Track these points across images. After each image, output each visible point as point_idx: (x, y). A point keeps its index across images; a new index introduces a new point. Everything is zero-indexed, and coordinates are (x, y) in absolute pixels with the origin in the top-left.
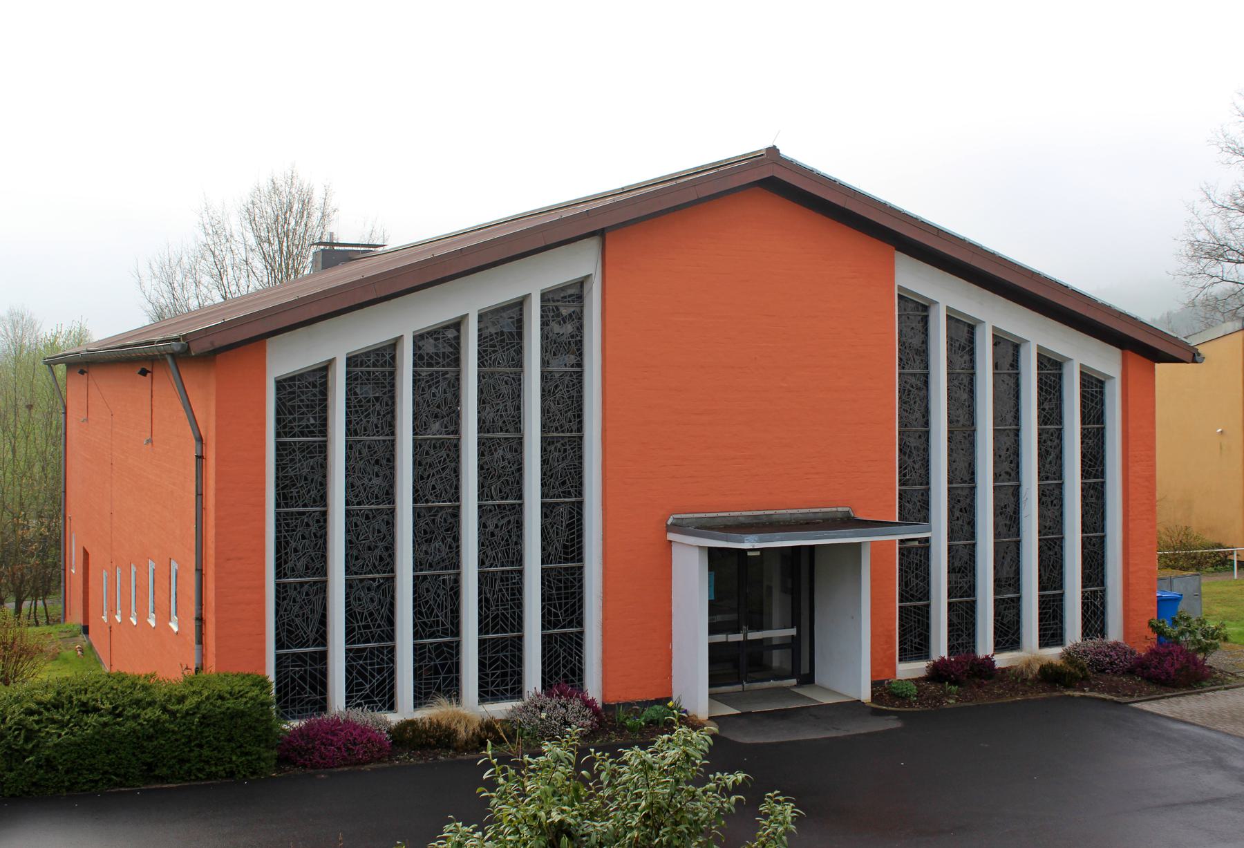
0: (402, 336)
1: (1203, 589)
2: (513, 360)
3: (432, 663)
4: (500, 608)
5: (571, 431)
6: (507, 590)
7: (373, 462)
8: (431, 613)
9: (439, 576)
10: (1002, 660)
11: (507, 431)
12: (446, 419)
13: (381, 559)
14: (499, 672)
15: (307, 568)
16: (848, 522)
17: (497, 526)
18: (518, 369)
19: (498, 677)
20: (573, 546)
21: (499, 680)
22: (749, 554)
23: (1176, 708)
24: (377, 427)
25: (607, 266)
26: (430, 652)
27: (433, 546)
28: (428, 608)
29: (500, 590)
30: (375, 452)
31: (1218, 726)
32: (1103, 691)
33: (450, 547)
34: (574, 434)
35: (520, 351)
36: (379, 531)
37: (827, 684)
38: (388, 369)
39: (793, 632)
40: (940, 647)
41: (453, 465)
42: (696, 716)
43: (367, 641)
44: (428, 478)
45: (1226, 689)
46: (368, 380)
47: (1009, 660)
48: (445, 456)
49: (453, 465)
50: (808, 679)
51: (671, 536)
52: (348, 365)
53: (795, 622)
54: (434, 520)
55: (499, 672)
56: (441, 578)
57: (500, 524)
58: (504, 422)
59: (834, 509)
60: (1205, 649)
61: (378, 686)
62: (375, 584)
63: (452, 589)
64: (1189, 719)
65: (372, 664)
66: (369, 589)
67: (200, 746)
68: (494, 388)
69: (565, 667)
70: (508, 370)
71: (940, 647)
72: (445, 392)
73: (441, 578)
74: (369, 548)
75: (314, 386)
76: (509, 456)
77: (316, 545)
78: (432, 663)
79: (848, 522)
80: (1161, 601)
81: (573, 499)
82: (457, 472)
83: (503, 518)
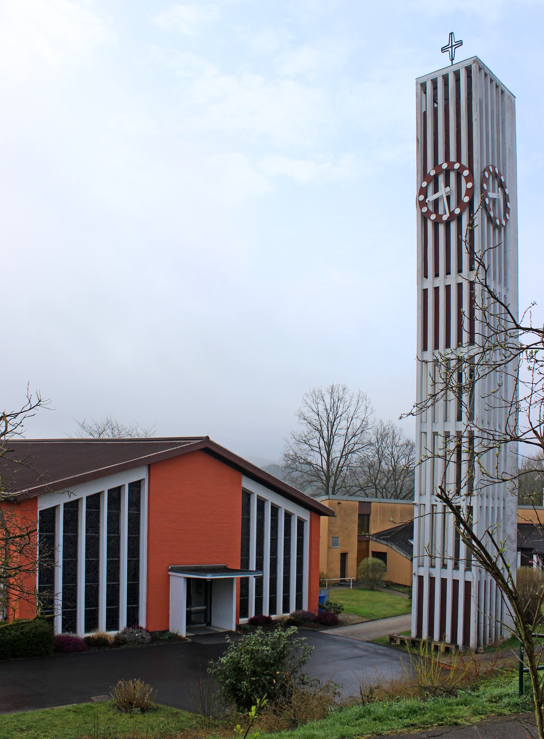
0: (82, 498)
1: (330, 593)
2: (117, 508)
3: (89, 617)
4: (112, 597)
5: (136, 535)
6: (114, 591)
7: (70, 543)
8: (89, 598)
9: (92, 585)
10: (273, 617)
11: (115, 534)
12: (94, 528)
13: (72, 579)
14: (111, 620)
15: (47, 581)
16: (225, 570)
17: (111, 568)
18: (118, 511)
19: (110, 622)
20: (136, 576)
21: (111, 623)
22: (207, 580)
23: (333, 632)
24: (71, 530)
25: (151, 476)
26: (88, 613)
27: (89, 574)
28: (88, 597)
29: (112, 591)
30: (71, 540)
31: (348, 637)
32: (308, 627)
33: (96, 575)
34: (137, 536)
35: (119, 504)
36: (72, 569)
37: (216, 625)
38: (75, 509)
39: (205, 607)
40: (252, 613)
41: (97, 545)
42: (182, 636)
43: (67, 608)
44: (88, 550)
45: (345, 626)
46: (69, 513)
47: (276, 617)
48: (94, 542)
49: (97, 545)
50: (209, 624)
51: (170, 573)
52: (64, 507)
53: (205, 604)
54: (90, 565)
55: (111, 620)
56: (92, 586)
57: (112, 567)
58: (114, 530)
59: (221, 565)
60: (338, 613)
61: (71, 625)
62: (70, 588)
63: (96, 590)
64: (338, 635)
65: (69, 617)
66: (68, 589)
67: (31, 645)
68: (111, 518)
69: (132, 619)
70: (115, 511)
71: (252, 613)
72: (95, 519)
73: (92, 586)
74: (69, 574)
75: (51, 514)
76: (115, 543)
77: (50, 573)
78: (89, 617)
79: (225, 570)
80: (320, 597)
81: (136, 559)
82: (98, 548)
83: (113, 565)
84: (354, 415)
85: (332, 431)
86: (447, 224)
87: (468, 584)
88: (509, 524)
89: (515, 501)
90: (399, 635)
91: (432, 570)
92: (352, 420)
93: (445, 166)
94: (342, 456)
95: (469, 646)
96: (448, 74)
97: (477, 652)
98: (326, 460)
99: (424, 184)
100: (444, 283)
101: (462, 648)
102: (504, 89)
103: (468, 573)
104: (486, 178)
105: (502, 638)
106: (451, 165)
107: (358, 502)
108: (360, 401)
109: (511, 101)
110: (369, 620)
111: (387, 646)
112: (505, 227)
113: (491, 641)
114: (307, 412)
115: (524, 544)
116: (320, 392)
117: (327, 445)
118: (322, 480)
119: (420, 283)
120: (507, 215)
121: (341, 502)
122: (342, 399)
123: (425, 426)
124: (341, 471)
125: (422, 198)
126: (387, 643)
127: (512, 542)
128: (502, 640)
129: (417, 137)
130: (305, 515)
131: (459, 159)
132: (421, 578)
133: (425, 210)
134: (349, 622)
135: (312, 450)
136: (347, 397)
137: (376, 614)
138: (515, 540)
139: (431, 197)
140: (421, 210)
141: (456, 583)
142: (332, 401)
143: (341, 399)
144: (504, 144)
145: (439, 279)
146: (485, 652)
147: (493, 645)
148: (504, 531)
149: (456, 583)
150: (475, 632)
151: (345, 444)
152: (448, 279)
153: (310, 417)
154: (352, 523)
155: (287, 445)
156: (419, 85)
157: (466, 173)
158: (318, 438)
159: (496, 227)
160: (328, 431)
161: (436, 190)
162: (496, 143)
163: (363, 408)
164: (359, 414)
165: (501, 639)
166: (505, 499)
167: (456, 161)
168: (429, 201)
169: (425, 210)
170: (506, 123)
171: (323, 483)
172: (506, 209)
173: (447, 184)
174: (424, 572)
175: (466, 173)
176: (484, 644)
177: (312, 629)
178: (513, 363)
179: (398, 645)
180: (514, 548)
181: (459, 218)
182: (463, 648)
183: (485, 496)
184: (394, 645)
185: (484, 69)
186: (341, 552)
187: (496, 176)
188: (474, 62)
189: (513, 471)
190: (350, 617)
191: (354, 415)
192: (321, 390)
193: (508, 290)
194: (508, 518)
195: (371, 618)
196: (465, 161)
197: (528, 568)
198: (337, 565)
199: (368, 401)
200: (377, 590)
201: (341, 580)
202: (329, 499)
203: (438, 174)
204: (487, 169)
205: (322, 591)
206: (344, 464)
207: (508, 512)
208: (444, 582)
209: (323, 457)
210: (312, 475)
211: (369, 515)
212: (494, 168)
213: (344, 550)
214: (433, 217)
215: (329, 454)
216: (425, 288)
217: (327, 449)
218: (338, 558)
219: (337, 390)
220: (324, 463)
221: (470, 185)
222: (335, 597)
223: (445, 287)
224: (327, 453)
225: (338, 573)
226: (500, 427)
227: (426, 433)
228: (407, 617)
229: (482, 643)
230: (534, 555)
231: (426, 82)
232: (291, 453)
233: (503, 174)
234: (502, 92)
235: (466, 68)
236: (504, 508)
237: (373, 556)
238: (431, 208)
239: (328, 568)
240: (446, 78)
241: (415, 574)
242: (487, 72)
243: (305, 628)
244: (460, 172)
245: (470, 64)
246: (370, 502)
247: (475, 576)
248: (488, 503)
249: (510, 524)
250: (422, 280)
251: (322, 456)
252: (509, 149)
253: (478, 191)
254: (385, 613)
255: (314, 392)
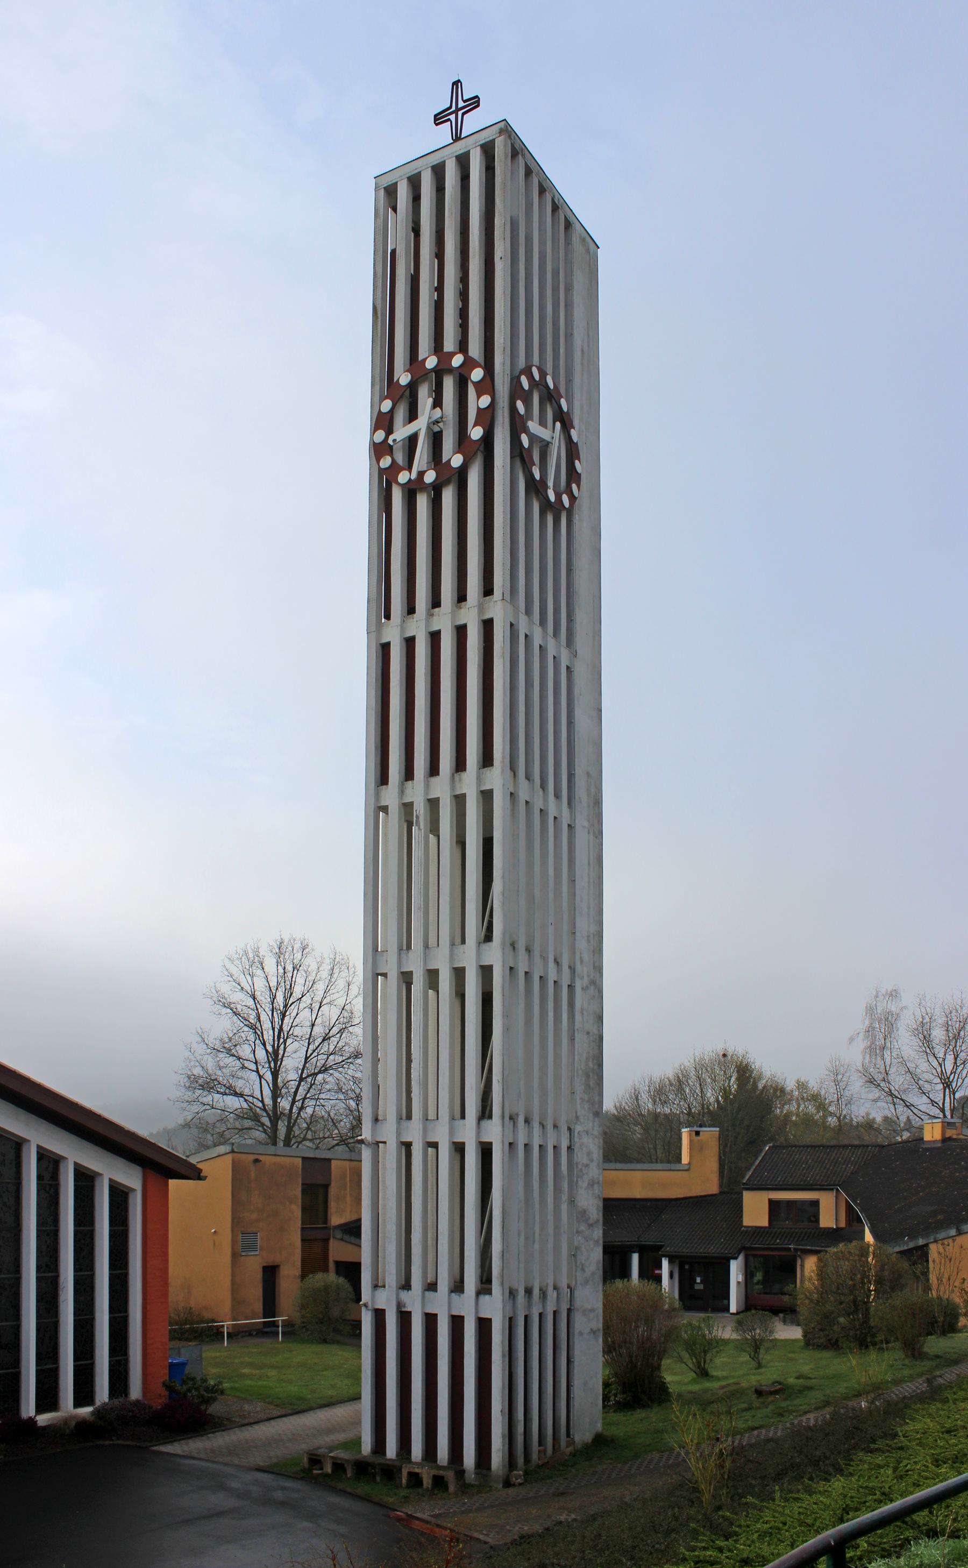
23: (186, 1448)
45: (223, 1431)
47: (49, 1420)
60: (209, 1401)
64: (196, 1455)
84: (324, 997)
85: (281, 1029)
86: (437, 489)
87: (484, 1326)
88: (583, 1184)
89: (596, 1133)
90: (331, 1451)
91: (404, 1295)
92: (320, 1007)
93: (431, 363)
94: (301, 1079)
95: (489, 1468)
96: (444, 162)
97: (507, 1484)
98: (271, 1085)
99: (387, 406)
100: (427, 625)
101: (473, 1476)
102: (572, 219)
103: (485, 1299)
104: (524, 389)
105: (571, 1442)
106: (446, 359)
107: (300, 1160)
108: (336, 971)
109: (588, 251)
110: (290, 1412)
111: (302, 1479)
112: (570, 512)
113: (542, 1452)
114: (231, 992)
115: (645, 1238)
116: (256, 952)
117: (272, 1057)
118: (263, 1125)
119: (374, 628)
120: (574, 486)
121: (261, 1158)
122: (300, 966)
123: (384, 958)
124: (302, 1108)
125: (380, 436)
126: (303, 1470)
127: (591, 1226)
128: (570, 1449)
129: (373, 304)
130: (131, 1178)
131: (463, 346)
132: (379, 1315)
133: (386, 462)
134: (237, 1420)
135: (243, 1067)
136: (310, 963)
137: (309, 1396)
138: (598, 1221)
139: (401, 433)
140: (378, 462)
141: (457, 1323)
142: (281, 971)
143: (298, 967)
144: (569, 336)
145: (415, 620)
146: (526, 1480)
147: (548, 1462)
148: (572, 1202)
149: (457, 1323)
150: (503, 1436)
151: (308, 1055)
152: (435, 618)
153: (239, 1004)
154: (288, 1203)
155: (192, 1057)
156: (382, 192)
157: (477, 374)
158: (251, 1043)
159: (546, 506)
160: (273, 1029)
161: (413, 415)
162: (549, 326)
163: (341, 984)
164: (334, 997)
165: (567, 1447)
166: (572, 1128)
167: (457, 350)
168: (394, 440)
169: (386, 462)
170: (575, 293)
171: (265, 1131)
172: (573, 476)
173: (438, 403)
174: (385, 1300)
175: (477, 374)
176: (527, 1460)
177: (135, 1443)
178: (589, 821)
179: (327, 1475)
180: (596, 1238)
181: (461, 476)
182: (476, 1474)
183: (521, 1119)
184: (319, 1475)
185: (523, 155)
186: (265, 1265)
187: (550, 397)
188: (501, 132)
189: (591, 1065)
190: (246, 1407)
191: (324, 997)
192: (259, 948)
193: (575, 655)
194: (581, 1170)
195: (295, 1407)
196: (475, 349)
197: (652, 1286)
198: (255, 1293)
199: (352, 971)
200: (333, 1342)
201: (264, 1322)
202: (233, 1151)
203: (417, 380)
204: (527, 372)
205: (183, 1351)
206: (308, 1096)
207: (580, 1157)
208: (431, 1321)
209: (263, 1081)
210: (243, 1117)
211: (326, 1187)
212: (543, 374)
213: (271, 1259)
214: (403, 477)
215: (275, 1074)
216: (384, 640)
217: (273, 1067)
218: (258, 1276)
219: (291, 949)
220: (267, 1093)
221: (485, 401)
222: (237, 1361)
223: (429, 635)
224: (272, 1073)
225: (259, 1307)
226: (558, 963)
227: (385, 975)
228: (339, 1413)
229: (521, 1460)
230: (663, 1259)
231: (396, 183)
232: (198, 1071)
233: (567, 391)
234: (568, 225)
235: (482, 146)
236: (569, 1148)
237: (338, 1273)
238: (400, 458)
239: (234, 1299)
240: (439, 171)
241: (365, 1305)
242: (532, 166)
243: (120, 1442)
244: (466, 375)
245: (491, 138)
246: (329, 1160)
247: (499, 1305)
248: (530, 1134)
249: (585, 1185)
250: (379, 624)
251: (261, 1077)
252: (582, 350)
253: (503, 415)
254: (331, 1392)
255: (246, 953)
